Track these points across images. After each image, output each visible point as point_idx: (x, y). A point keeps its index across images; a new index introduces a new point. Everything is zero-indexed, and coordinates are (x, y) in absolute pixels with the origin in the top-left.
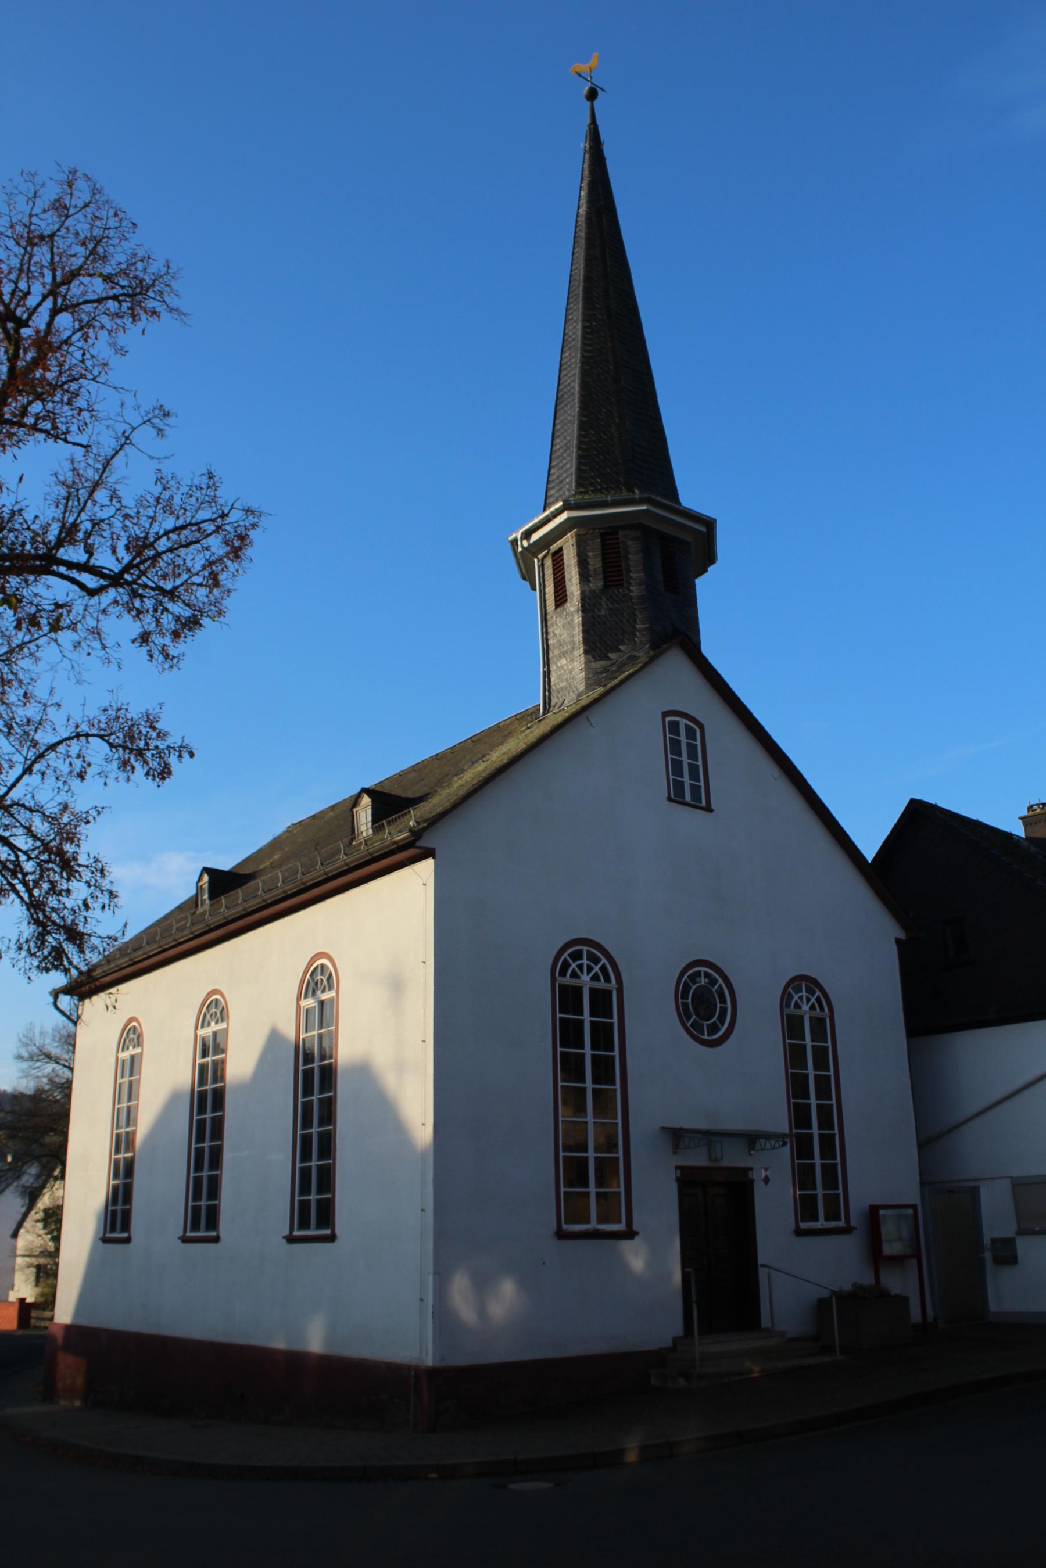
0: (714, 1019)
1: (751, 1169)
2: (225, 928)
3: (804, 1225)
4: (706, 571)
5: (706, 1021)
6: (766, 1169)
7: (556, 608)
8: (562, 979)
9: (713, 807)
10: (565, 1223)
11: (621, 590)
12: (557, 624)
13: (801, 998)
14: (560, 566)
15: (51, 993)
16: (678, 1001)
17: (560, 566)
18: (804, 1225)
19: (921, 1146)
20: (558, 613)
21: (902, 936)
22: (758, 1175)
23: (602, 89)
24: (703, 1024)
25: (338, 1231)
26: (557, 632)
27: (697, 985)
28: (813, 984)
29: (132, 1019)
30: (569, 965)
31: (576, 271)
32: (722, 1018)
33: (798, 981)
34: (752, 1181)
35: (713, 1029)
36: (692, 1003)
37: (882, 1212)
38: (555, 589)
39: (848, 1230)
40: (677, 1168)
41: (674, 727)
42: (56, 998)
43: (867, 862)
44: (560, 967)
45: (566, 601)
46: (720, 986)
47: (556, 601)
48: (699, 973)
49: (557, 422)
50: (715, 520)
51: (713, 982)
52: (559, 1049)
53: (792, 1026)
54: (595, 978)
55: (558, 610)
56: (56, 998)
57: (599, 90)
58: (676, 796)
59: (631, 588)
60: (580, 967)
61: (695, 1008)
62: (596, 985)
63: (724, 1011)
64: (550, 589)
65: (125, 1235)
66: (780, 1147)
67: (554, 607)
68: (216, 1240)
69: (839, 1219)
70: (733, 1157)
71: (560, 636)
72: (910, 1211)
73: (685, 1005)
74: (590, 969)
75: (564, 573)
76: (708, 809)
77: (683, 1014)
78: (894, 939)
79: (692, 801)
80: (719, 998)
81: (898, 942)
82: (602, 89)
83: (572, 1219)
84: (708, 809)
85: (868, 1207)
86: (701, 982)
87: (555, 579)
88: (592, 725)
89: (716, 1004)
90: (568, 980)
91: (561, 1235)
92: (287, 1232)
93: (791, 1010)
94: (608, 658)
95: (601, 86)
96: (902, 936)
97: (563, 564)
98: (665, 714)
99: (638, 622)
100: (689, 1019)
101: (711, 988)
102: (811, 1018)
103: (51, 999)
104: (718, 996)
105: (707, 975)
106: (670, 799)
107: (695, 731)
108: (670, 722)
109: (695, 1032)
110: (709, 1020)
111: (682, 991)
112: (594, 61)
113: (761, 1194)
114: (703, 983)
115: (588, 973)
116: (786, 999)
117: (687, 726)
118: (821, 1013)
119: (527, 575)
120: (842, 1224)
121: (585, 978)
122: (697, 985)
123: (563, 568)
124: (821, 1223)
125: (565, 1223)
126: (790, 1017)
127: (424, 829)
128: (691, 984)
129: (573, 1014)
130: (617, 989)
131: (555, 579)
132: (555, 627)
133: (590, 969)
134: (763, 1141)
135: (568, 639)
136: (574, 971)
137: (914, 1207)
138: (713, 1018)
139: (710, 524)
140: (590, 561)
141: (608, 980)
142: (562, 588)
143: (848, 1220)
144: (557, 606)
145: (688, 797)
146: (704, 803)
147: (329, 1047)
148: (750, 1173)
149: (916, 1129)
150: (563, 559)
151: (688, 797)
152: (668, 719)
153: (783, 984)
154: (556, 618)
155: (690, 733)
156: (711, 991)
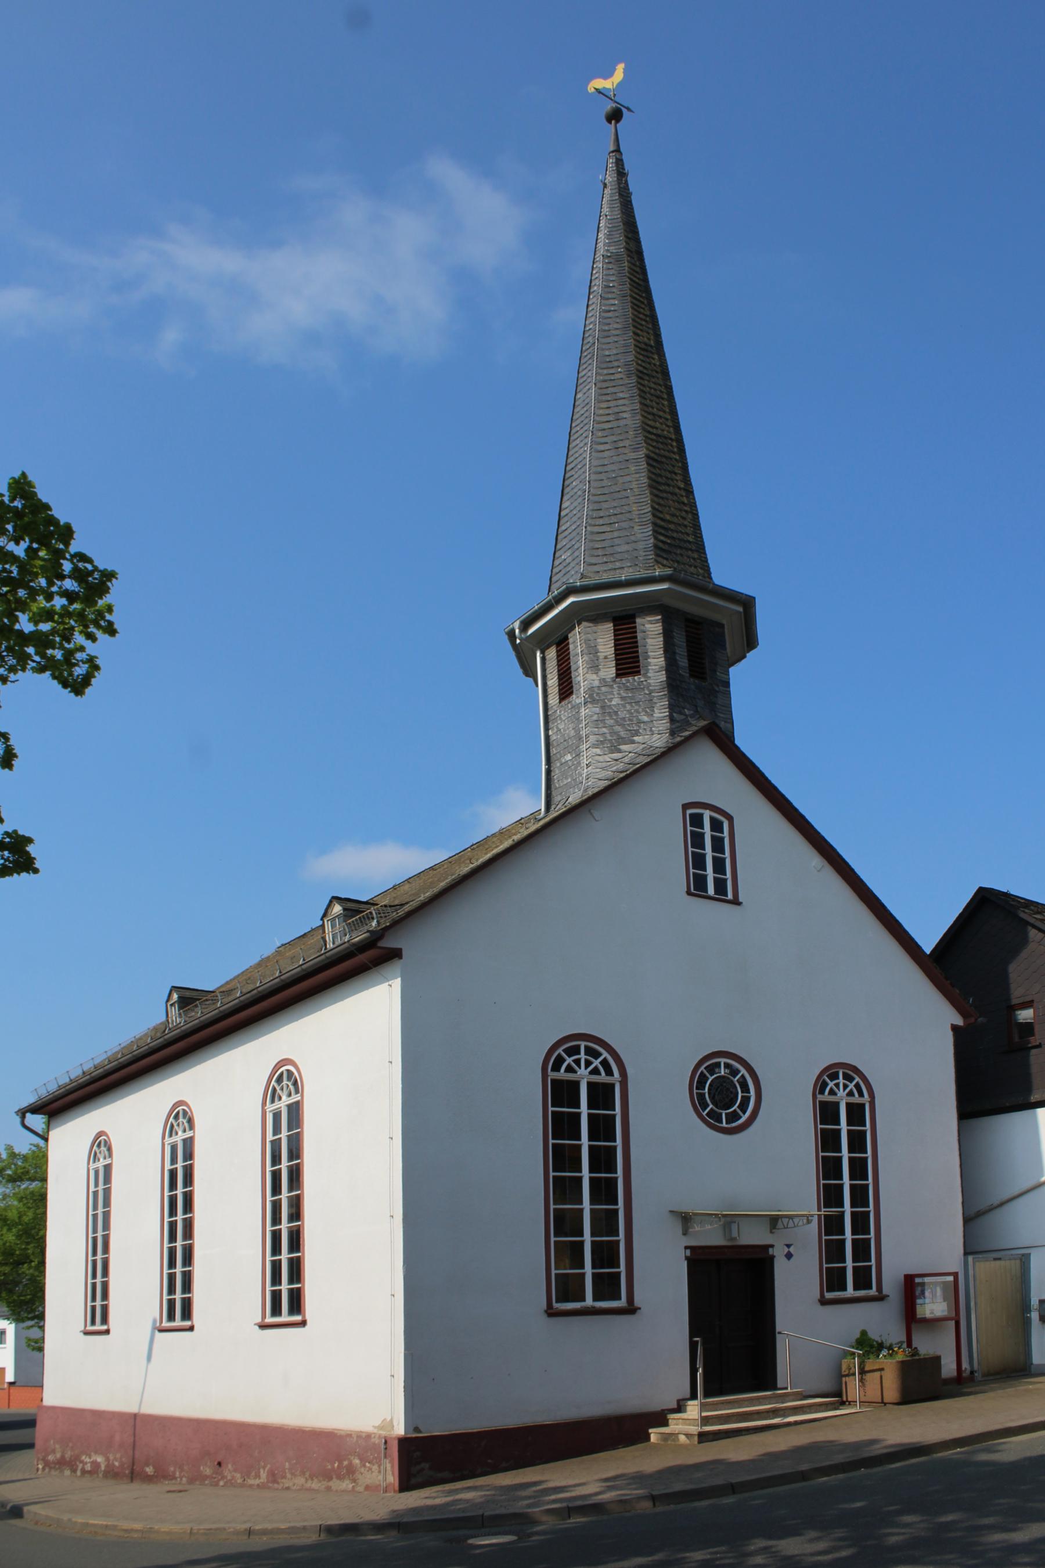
0: (735, 1107)
1: (772, 1246)
2: (186, 1041)
3: (829, 1295)
4: (744, 657)
5: (726, 1110)
6: (788, 1246)
7: (560, 702)
8: (555, 1074)
9: (741, 900)
10: (557, 1302)
11: (636, 678)
12: (561, 719)
13: (837, 1085)
14: (566, 656)
15: (17, 1113)
16: (817, 1127)
17: (566, 656)
18: (829, 1295)
19: (968, 1220)
20: (562, 706)
21: (959, 1021)
22: (778, 1253)
23: (628, 109)
24: (721, 1114)
25: (308, 1317)
26: (561, 727)
27: (715, 1076)
28: (851, 1072)
29: (101, 1134)
30: (564, 1060)
31: (591, 326)
32: (744, 1107)
33: (831, 1072)
34: (772, 1258)
35: (733, 1117)
36: (709, 1093)
37: (917, 1280)
38: (559, 682)
39: (880, 1298)
40: (686, 1248)
41: (697, 821)
42: (23, 1117)
43: (925, 953)
44: (553, 1061)
45: (571, 693)
46: (743, 1076)
47: (560, 695)
48: (718, 1065)
49: (565, 498)
50: (754, 598)
51: (734, 1072)
52: (551, 1141)
53: (827, 1113)
54: (851, 1094)
55: (563, 703)
56: (23, 1117)
57: (624, 110)
58: (697, 887)
59: (649, 675)
60: (577, 1062)
61: (712, 1098)
62: (595, 1078)
63: (746, 1101)
64: (553, 681)
65: (105, 1327)
66: (804, 1225)
67: (558, 701)
68: (191, 1329)
69: (870, 1288)
70: (751, 1236)
71: (565, 730)
72: (951, 1278)
73: (701, 1097)
74: (588, 1064)
75: (570, 663)
76: (736, 902)
77: (699, 1103)
78: (950, 1025)
79: (715, 894)
80: (741, 1088)
81: (955, 1028)
82: (628, 109)
83: (563, 1297)
84: (736, 902)
85: (903, 1278)
86: (720, 1073)
87: (559, 671)
88: (595, 819)
89: (737, 1093)
90: (562, 1074)
91: (551, 1313)
92: (259, 1320)
93: (826, 1097)
94: (620, 751)
95: (626, 105)
96: (959, 1021)
97: (569, 653)
98: (685, 807)
99: (656, 711)
100: (704, 1108)
101: (732, 1078)
102: (848, 1105)
103: (18, 1119)
104: (740, 1085)
105: (727, 1066)
106: (689, 893)
107: (721, 823)
108: (691, 815)
109: (712, 1121)
110: (728, 1109)
111: (698, 1081)
112: (619, 75)
113: (781, 1269)
114: (723, 1073)
115: (586, 1068)
116: (820, 1086)
117: (712, 819)
118: (861, 1099)
119: (529, 671)
120: (873, 1292)
121: (841, 1093)
122: (715, 1076)
123: (569, 658)
124: (285, 1318)
125: (827, 1291)
126: (823, 1104)
127: (387, 929)
128: (708, 1075)
129: (568, 1107)
130: (620, 1082)
131: (559, 671)
132: (559, 722)
133: (588, 1064)
134: (785, 1220)
135: (572, 733)
136: (569, 1065)
137: (955, 1275)
138: (733, 1106)
139: (747, 604)
140: (600, 648)
141: (609, 1072)
142: (567, 680)
143: (880, 1288)
144: (561, 700)
145: (711, 891)
146: (730, 896)
147: (296, 1148)
148: (770, 1250)
149: (963, 1203)
150: (569, 649)
151: (711, 891)
152: (689, 812)
153: (817, 1072)
154: (560, 712)
155: (716, 826)
156: (732, 1082)
